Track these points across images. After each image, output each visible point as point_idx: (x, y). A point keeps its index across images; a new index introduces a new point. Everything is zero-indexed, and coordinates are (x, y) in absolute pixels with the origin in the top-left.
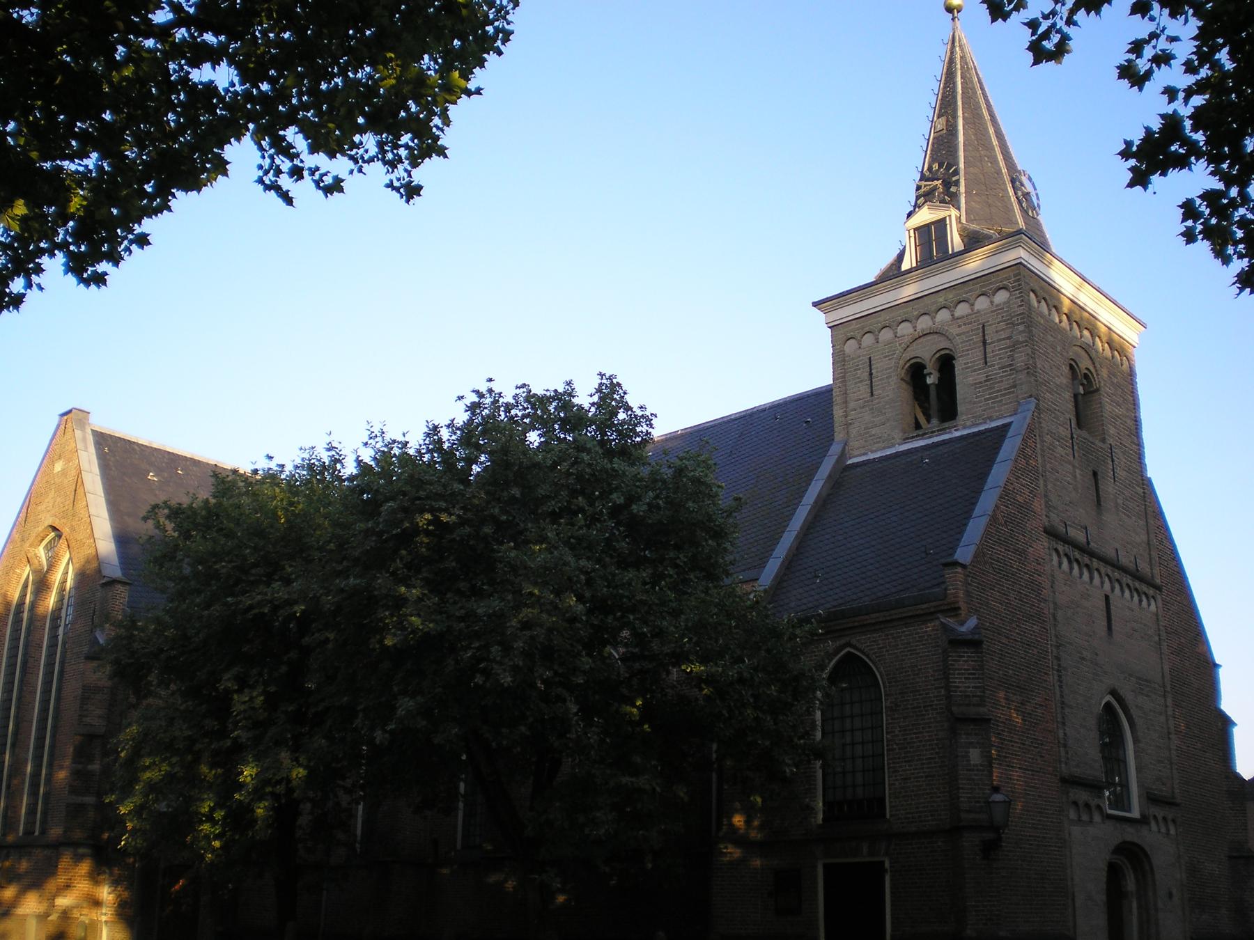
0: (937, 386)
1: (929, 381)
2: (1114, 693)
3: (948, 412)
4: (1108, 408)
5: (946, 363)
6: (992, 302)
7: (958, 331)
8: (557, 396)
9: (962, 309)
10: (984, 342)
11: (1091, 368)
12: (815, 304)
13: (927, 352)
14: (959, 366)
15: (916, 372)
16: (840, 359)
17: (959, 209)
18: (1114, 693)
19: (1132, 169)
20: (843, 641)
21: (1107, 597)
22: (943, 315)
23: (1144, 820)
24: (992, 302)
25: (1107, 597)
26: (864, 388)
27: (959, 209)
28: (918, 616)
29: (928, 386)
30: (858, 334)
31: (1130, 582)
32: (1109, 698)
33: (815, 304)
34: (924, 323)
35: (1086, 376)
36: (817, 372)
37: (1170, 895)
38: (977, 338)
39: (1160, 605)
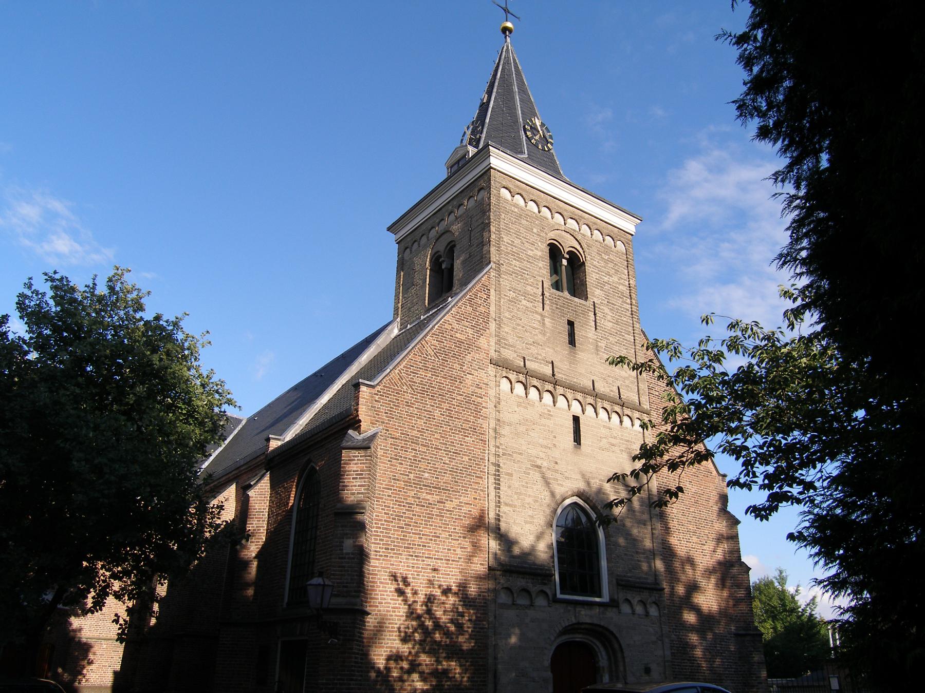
11: (579, 248)
21: (576, 419)
23: (613, 603)
25: (576, 419)
32: (575, 499)
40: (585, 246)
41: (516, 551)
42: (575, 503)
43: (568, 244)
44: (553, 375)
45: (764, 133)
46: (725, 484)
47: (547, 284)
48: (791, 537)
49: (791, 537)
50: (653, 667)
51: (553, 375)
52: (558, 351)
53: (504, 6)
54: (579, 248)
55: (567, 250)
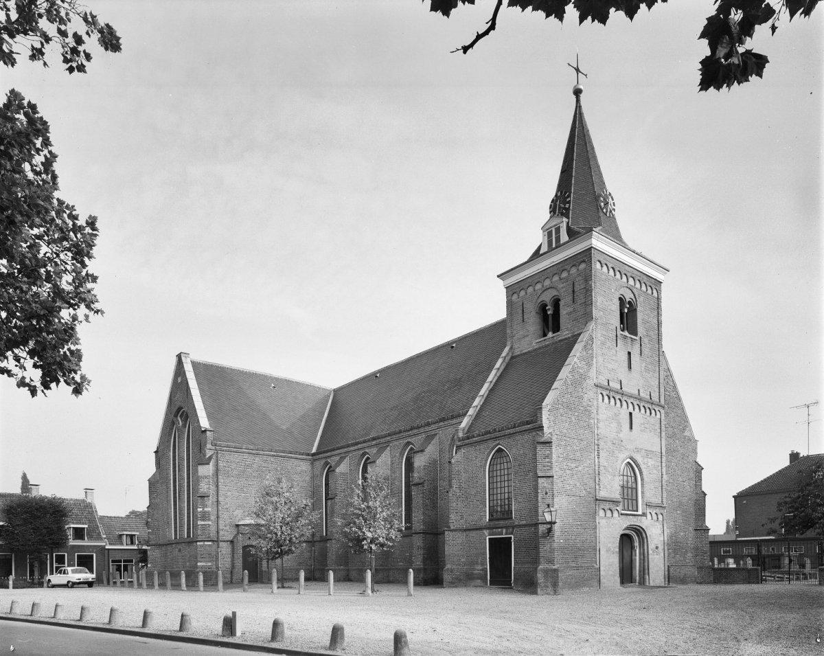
0: (552, 315)
1: (549, 313)
2: (631, 458)
3: (556, 328)
4: (286, 631)
5: (556, 303)
6: (578, 269)
7: (562, 285)
8: (511, 290)
9: (564, 275)
10: (573, 291)
11: (634, 299)
12: (498, 276)
13: (547, 297)
14: (562, 303)
15: (543, 307)
16: (510, 304)
17: (568, 218)
18: (631, 458)
19: (38, 113)
20: (497, 442)
21: (631, 414)
22: (556, 278)
23: (644, 514)
24: (578, 269)
25: (631, 414)
26: (577, 288)
27: (568, 218)
28: (526, 430)
29: (548, 315)
30: (518, 290)
31: (650, 406)
32: (629, 460)
33: (498, 276)
34: (547, 283)
35: (629, 303)
36: (500, 313)
37: (657, 548)
38: (571, 290)
39: (663, 415)
40: (637, 297)
41: (34, 493)
42: (628, 462)
43: (628, 296)
44: (621, 389)
45: (729, 86)
46: (84, 322)
47: (619, 328)
48: (24, 478)
49: (24, 478)
50: (659, 546)
51: (639, 395)
52: (622, 372)
53: (576, 66)
54: (634, 299)
55: (627, 300)
